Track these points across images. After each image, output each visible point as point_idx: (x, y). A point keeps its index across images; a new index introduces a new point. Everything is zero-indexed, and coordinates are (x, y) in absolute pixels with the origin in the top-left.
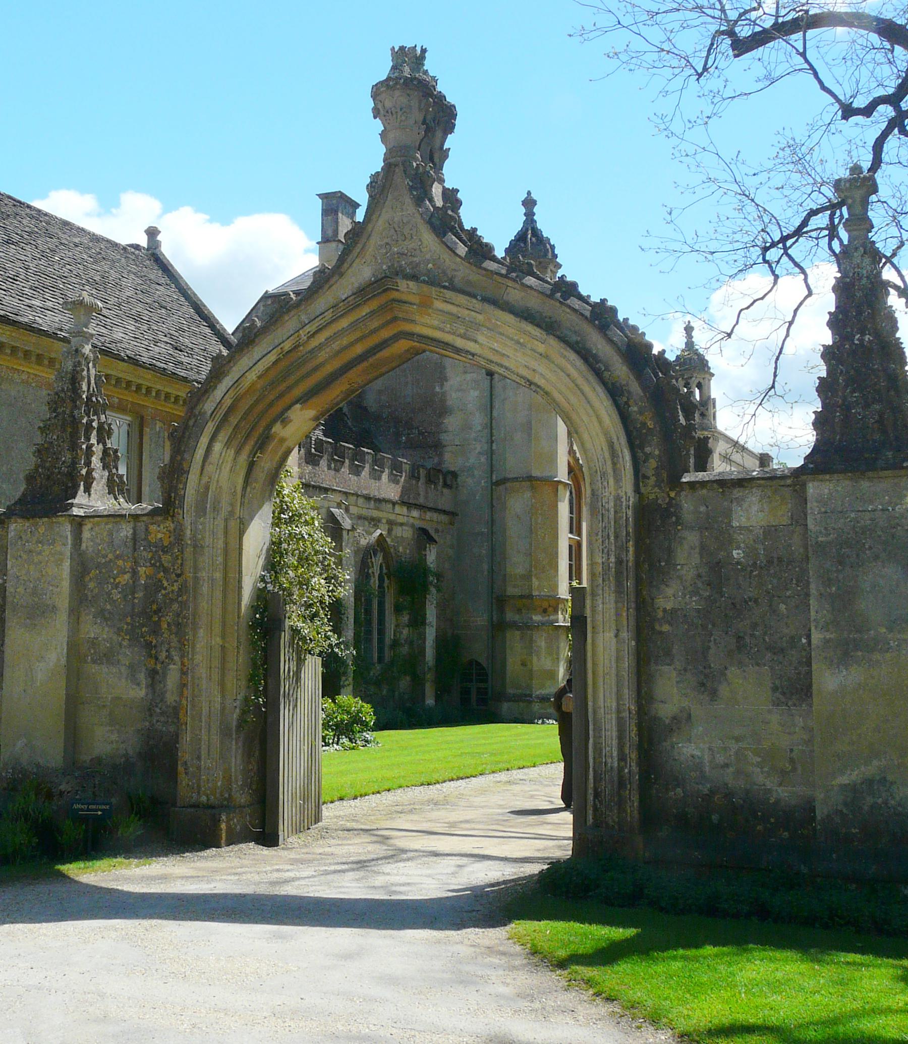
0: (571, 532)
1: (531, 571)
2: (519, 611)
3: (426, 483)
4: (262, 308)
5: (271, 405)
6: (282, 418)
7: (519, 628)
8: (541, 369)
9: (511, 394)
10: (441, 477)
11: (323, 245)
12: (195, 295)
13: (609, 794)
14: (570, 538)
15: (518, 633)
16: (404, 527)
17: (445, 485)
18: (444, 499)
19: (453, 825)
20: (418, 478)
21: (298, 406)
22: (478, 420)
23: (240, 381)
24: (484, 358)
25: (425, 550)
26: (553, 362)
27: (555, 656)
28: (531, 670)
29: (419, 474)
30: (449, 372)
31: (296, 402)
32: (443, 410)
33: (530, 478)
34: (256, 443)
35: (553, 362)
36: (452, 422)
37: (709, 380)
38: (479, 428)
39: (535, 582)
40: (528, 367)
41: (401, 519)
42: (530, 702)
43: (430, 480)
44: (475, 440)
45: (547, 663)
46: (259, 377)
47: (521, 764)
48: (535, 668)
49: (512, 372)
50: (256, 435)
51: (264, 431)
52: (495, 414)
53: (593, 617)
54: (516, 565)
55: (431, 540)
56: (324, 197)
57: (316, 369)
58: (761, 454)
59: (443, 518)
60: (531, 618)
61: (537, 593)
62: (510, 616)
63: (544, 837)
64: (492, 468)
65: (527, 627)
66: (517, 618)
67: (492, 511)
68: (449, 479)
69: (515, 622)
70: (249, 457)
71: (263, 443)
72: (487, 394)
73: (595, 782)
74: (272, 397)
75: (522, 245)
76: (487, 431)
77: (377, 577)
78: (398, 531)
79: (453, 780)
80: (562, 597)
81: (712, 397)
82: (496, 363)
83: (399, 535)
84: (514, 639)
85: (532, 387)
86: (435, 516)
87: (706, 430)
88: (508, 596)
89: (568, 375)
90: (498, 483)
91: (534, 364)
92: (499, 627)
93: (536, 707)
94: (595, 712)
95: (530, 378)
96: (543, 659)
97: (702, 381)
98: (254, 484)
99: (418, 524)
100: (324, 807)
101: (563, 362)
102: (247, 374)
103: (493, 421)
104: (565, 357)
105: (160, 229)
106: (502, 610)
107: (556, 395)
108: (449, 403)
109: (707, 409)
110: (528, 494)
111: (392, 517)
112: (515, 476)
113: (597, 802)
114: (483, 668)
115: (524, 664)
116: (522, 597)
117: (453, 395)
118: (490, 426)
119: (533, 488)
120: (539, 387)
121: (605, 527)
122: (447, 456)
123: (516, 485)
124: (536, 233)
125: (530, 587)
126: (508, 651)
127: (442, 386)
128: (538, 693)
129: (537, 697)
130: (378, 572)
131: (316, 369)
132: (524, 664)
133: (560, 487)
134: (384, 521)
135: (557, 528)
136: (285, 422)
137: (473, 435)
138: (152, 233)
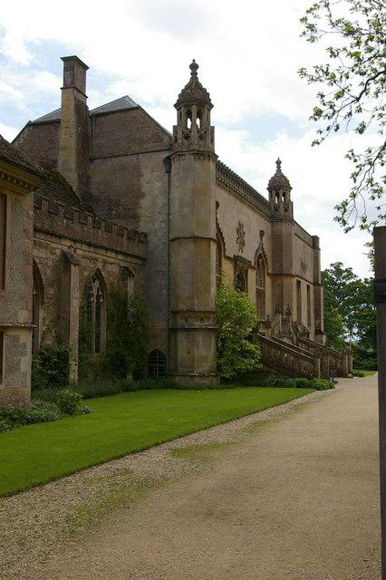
2: (186, 319)
7: (185, 330)
17: (140, 241)
18: (138, 250)
22: (161, 201)
28: (193, 357)
30: (144, 171)
32: (140, 195)
36: (145, 203)
37: (209, 110)
48: (196, 355)
54: (184, 290)
55: (131, 275)
56: (64, 59)
62: (180, 322)
68: (143, 238)
78: (109, 267)
84: (182, 338)
92: (173, 331)
96: (200, 348)
99: (122, 264)
105: (363, 135)
106: (175, 318)
108: (143, 190)
110: (192, 246)
114: (163, 354)
115: (189, 352)
119: (195, 241)
122: (141, 223)
125: (193, 304)
138: (194, 101)
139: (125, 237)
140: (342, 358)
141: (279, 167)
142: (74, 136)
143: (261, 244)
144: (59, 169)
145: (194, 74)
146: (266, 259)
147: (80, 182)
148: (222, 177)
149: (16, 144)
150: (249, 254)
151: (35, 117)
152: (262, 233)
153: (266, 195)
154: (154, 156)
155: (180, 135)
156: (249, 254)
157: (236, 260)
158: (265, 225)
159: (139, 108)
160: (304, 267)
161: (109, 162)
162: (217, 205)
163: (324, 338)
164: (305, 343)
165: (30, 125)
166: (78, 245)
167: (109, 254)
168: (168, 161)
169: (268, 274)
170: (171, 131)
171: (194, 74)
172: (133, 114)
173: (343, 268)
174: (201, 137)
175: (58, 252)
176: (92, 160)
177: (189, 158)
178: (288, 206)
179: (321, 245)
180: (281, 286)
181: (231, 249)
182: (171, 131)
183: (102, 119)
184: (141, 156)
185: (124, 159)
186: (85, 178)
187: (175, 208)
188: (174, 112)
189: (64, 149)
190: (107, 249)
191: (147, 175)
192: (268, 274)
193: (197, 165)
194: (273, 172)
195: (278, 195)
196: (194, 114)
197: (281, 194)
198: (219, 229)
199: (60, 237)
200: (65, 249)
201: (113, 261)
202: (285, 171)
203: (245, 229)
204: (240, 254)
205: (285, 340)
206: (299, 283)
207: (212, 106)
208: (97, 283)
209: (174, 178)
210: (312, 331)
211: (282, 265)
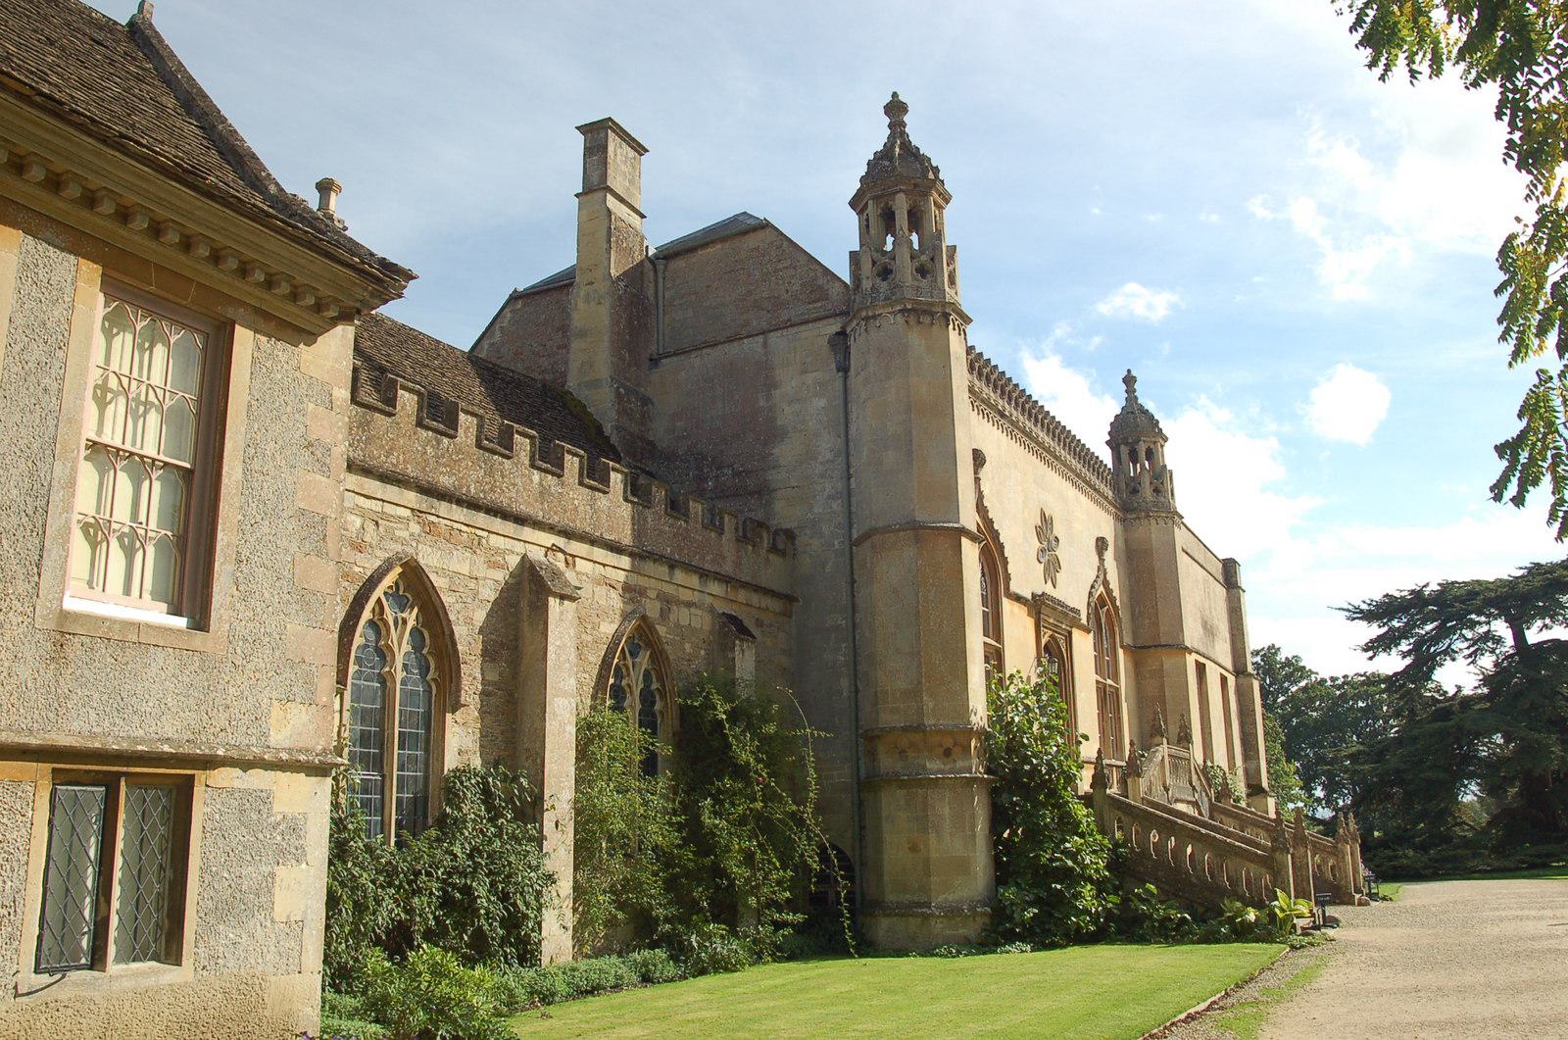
0: (986, 634)
1: (920, 683)
3: (738, 540)
4: (509, 315)
7: (902, 784)
10: (765, 535)
11: (585, 198)
12: (190, 78)
14: (985, 643)
15: (901, 793)
16: (693, 610)
18: (772, 572)
20: (720, 531)
22: (827, 444)
25: (732, 649)
28: (927, 860)
29: (722, 523)
32: (773, 434)
36: (785, 452)
37: (1162, 446)
38: (829, 456)
39: (929, 704)
41: (686, 595)
42: (926, 917)
43: (745, 536)
44: (822, 476)
48: (934, 855)
54: (893, 675)
56: (584, 129)
59: (774, 604)
60: (924, 767)
64: (850, 518)
65: (916, 783)
67: (852, 587)
68: (784, 542)
69: (897, 774)
72: (839, 402)
75: (887, 163)
76: (841, 459)
77: (637, 693)
78: (682, 616)
81: (1169, 468)
83: (684, 621)
84: (892, 805)
86: (756, 599)
88: (882, 729)
93: (938, 927)
97: (1152, 446)
99: (722, 607)
100: (1317, 816)
106: (872, 754)
109: (1162, 483)
111: (669, 589)
115: (914, 849)
116: (905, 729)
117: (787, 408)
119: (918, 540)
122: (778, 506)
124: (912, 153)
125: (920, 712)
127: (769, 397)
130: (641, 686)
132: (914, 849)
134: (652, 594)
139: (729, 534)
142: (607, 302)
143: (1102, 569)
144: (572, 384)
145: (897, 127)
147: (622, 412)
148: (987, 392)
149: (486, 344)
150: (1073, 591)
151: (527, 279)
152: (1101, 545)
154: (806, 332)
155: (867, 267)
156: (1073, 591)
157: (1037, 606)
158: (1105, 524)
159: (765, 225)
160: (1209, 630)
161: (695, 360)
162: (979, 458)
163: (1271, 802)
164: (1235, 816)
165: (515, 297)
166: (577, 547)
167: (679, 576)
168: (841, 342)
170: (845, 275)
171: (897, 127)
172: (752, 241)
173: (1281, 657)
174: (922, 271)
175: (514, 561)
176: (654, 361)
177: (892, 322)
178: (1161, 479)
180: (1160, 673)
181: (1026, 576)
182: (845, 275)
183: (679, 264)
184: (774, 338)
185: (733, 349)
186: (634, 399)
187: (862, 457)
188: (853, 219)
189: (583, 334)
190: (672, 565)
191: (789, 382)
193: (915, 339)
195: (1134, 457)
196: (902, 220)
197: (1142, 454)
198: (981, 509)
199: (520, 520)
200: (537, 554)
201: (695, 597)
203: (1059, 530)
204: (1048, 589)
205: (1181, 807)
206: (1201, 669)
207: (1166, 440)
208: (644, 659)
209: (855, 381)
210: (1240, 788)
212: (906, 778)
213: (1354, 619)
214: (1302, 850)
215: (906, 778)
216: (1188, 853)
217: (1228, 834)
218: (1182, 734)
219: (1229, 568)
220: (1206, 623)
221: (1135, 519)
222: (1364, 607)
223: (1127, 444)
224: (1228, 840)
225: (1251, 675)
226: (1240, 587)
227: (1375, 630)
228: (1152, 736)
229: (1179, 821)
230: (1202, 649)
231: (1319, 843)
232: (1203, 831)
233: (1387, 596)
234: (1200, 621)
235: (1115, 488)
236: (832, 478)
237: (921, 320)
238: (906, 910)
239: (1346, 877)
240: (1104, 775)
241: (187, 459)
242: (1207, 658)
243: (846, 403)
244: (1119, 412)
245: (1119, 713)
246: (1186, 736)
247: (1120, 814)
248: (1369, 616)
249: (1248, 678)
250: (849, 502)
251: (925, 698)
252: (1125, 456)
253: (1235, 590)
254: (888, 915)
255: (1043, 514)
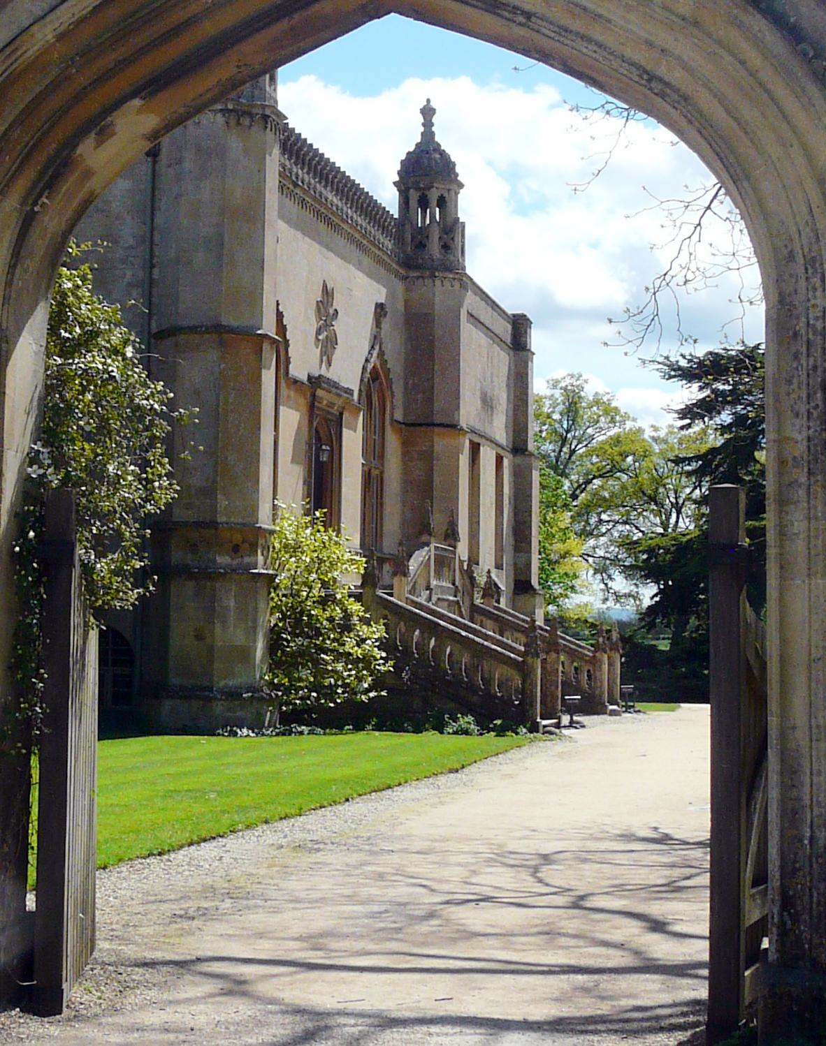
1: (214, 482)
2: (194, 548)
5: (79, 97)
6: (98, 125)
7: (191, 576)
8: (682, 47)
9: (190, 187)
13: (819, 903)
15: (191, 584)
19: (314, 940)
21: (137, 102)
23: (18, 42)
24: (551, 23)
26: (710, 36)
27: (250, 624)
28: (211, 649)
31: (133, 95)
33: (219, 329)
34: (42, 174)
35: (710, 36)
37: (457, 194)
38: (131, 241)
39: (222, 502)
40: (650, 44)
42: (209, 700)
44: (123, 261)
45: (237, 636)
46: (61, 37)
47: (282, 811)
49: (611, 53)
50: (42, 157)
51: (58, 152)
52: (159, 220)
53: (781, 546)
57: (177, 30)
58: (514, 316)
60: (214, 561)
61: (224, 519)
62: (177, 555)
63: (530, 968)
65: (207, 575)
66: (189, 559)
70: (23, 203)
71: (50, 180)
73: (782, 877)
74: (83, 81)
79: (191, 844)
80: (263, 526)
81: (461, 221)
82: (577, 34)
85: (653, 85)
87: (451, 271)
89: (742, 63)
90: (162, 335)
91: (663, 37)
93: (219, 708)
94: (783, 737)
95: (649, 68)
97: (446, 195)
98: (28, 261)
101: (733, 35)
102: (34, 28)
103: (155, 233)
104: (740, 26)
107: (705, 100)
109: (453, 239)
110: (213, 355)
112: (192, 324)
113: (787, 918)
115: (199, 637)
118: (149, 240)
119: (222, 344)
120: (668, 84)
121: (815, 368)
123: (195, 338)
126: (173, 615)
128: (222, 683)
129: (221, 691)
131: (177, 30)
133: (266, 346)
135: (260, 412)
136: (104, 134)
137: (120, 253)
140: (594, 661)
141: (428, 124)
146: (390, 382)
153: (389, 199)
160: (487, 403)
169: (394, 422)
178: (451, 231)
179: (537, 339)
180: (428, 457)
181: (304, 362)
182: (396, 216)
192: (394, 422)
193: (234, 143)
194: (410, 140)
202: (443, 139)
203: (339, 303)
204: (323, 371)
206: (475, 448)
207: (461, 186)
210: (503, 581)
211: (430, 400)
212: (196, 570)
213: (671, 377)
214: (554, 655)
215: (196, 570)
216: (448, 653)
217: (487, 637)
218: (449, 532)
219: (520, 325)
220: (486, 395)
221: (418, 278)
222: (683, 363)
223: (418, 189)
224: (486, 643)
225: (531, 455)
226: (529, 350)
227: (692, 393)
228: (421, 533)
229: (442, 623)
230: (478, 426)
231: (577, 651)
232: (464, 633)
233: (711, 353)
234: (478, 393)
235: (399, 240)
236: (133, 265)
237: (241, 121)
238: (188, 694)
239: (601, 687)
240: (374, 576)
241: (456, 613)
242: (482, 436)
243: (153, 195)
244: (412, 148)
245: (382, 498)
246: (453, 534)
247: (387, 612)
248: (688, 375)
249: (527, 458)
250: (150, 293)
251: (219, 496)
252: (413, 203)
253: (525, 353)
254: (172, 697)
255: (325, 286)
